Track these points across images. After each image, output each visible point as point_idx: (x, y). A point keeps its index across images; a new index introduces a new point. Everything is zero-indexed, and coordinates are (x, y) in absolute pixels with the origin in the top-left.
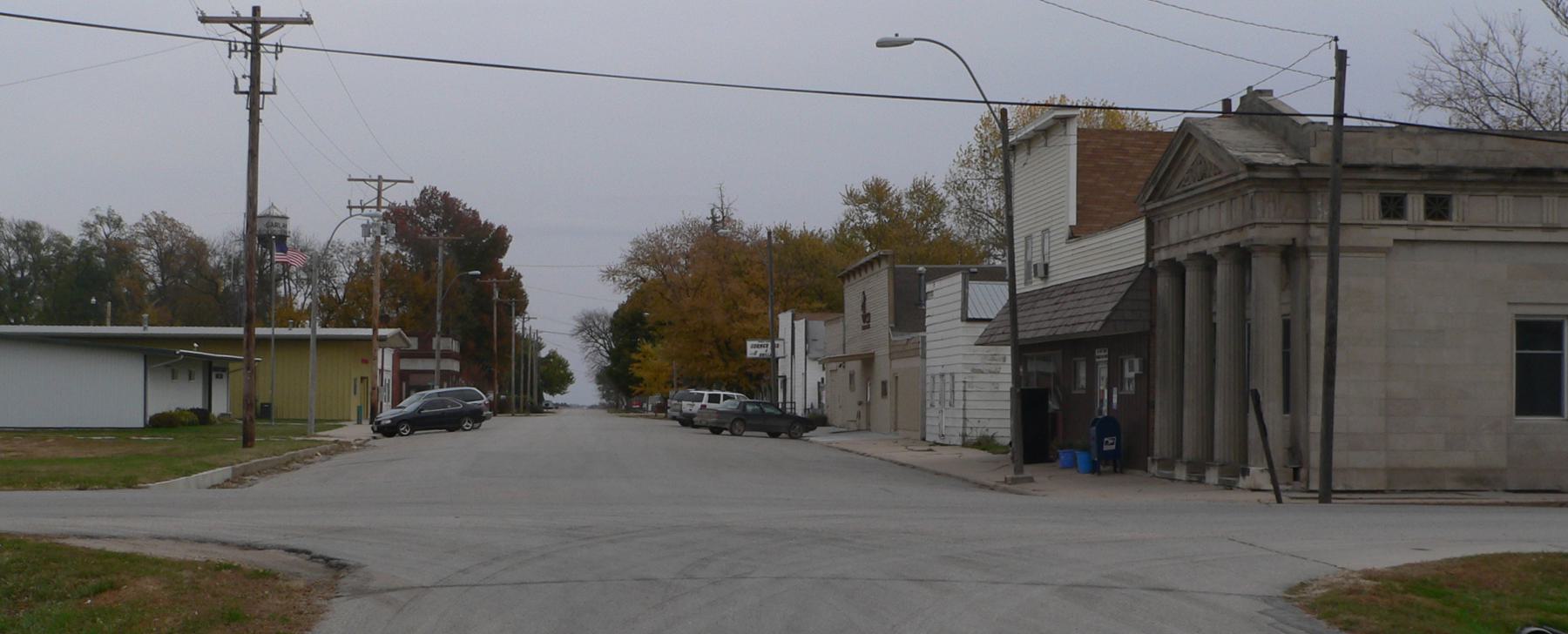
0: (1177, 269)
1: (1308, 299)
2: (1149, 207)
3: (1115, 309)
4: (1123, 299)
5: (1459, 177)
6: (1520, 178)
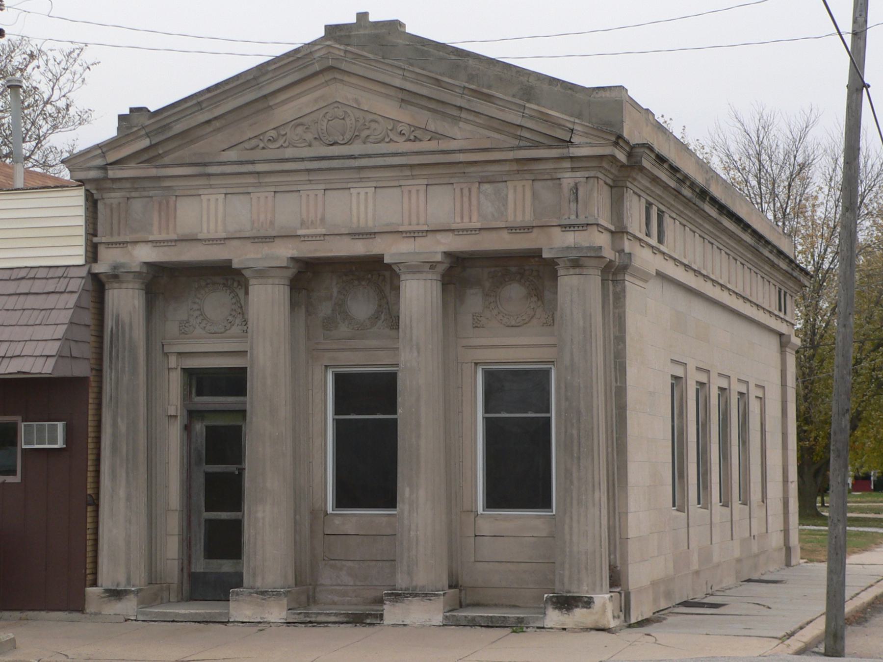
2: (111, 174)
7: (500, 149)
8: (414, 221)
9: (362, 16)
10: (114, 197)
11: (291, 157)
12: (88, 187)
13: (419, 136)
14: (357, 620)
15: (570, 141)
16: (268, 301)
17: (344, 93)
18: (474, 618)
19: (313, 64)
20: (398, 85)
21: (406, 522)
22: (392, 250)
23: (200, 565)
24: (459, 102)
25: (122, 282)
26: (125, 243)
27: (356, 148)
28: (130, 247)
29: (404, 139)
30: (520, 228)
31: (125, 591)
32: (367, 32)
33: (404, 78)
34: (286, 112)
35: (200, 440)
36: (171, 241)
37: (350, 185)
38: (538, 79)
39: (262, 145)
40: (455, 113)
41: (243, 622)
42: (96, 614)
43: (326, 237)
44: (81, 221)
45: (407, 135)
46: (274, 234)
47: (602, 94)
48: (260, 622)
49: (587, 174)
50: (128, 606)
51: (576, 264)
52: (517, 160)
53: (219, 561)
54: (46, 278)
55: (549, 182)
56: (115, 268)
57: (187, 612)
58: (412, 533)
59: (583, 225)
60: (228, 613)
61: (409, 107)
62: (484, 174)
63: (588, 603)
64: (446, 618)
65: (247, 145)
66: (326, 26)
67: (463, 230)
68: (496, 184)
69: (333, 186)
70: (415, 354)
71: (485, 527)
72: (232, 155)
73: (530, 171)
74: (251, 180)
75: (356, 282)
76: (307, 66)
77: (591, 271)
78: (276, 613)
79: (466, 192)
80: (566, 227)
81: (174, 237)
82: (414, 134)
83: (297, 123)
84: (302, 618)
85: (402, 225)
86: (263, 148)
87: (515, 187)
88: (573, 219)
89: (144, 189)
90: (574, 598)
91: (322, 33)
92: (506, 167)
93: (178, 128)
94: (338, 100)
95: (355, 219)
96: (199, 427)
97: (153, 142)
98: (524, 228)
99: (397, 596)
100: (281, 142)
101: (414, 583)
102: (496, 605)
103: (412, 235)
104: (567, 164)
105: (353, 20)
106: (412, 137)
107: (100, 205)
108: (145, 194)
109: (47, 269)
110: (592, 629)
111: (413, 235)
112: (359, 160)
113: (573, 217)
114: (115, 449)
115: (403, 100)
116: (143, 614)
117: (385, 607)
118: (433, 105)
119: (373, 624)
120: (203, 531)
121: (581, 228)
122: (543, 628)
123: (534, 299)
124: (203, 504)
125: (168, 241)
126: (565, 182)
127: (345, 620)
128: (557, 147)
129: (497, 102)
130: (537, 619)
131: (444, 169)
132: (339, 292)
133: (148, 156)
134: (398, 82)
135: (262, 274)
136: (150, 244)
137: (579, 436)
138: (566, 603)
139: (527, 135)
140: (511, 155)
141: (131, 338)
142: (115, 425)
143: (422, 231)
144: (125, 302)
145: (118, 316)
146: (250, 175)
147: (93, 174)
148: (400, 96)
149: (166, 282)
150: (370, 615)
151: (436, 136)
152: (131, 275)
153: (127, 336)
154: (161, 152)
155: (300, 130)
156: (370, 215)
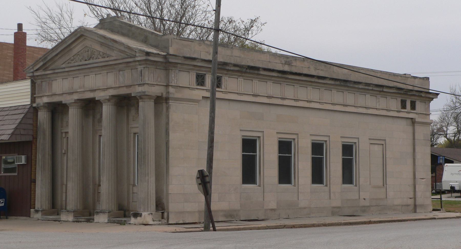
0: (57, 110)
1: (168, 124)
2: (36, 74)
3: (16, 128)
4: (20, 123)
5: (227, 68)
6: (248, 71)
23: (212, 229)
27: (91, 61)
33: (98, 37)
34: (75, 51)
44: (29, 90)
50: (39, 215)
64: (108, 220)
65: (67, 62)
77: (146, 100)
78: (71, 218)
80: (139, 85)
88: (141, 83)
92: (123, 65)
93: (49, 58)
111: (104, 90)
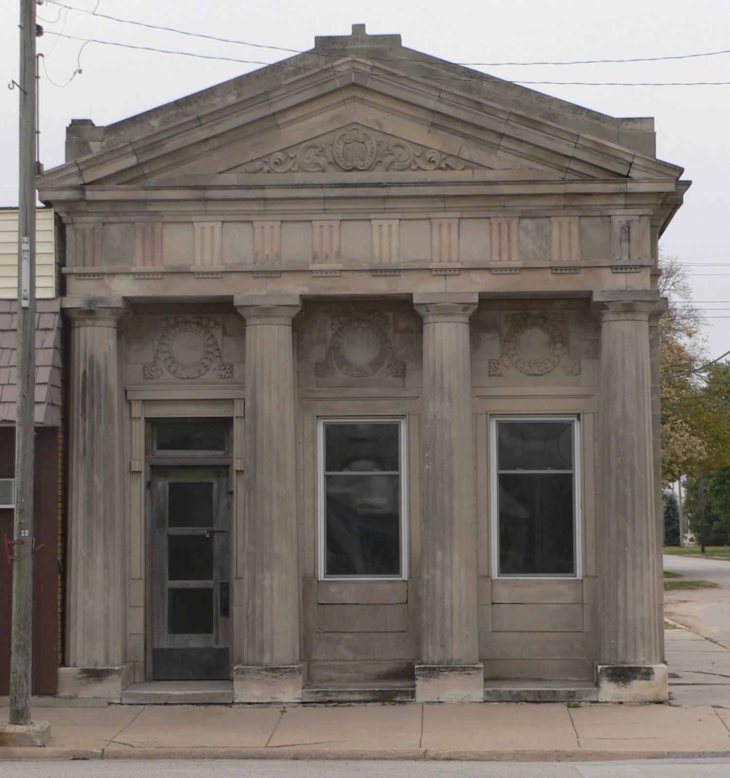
2: (89, 195)
7: (550, 182)
8: (445, 257)
9: (359, 28)
10: (87, 222)
11: (301, 182)
12: (58, 210)
13: (451, 164)
14: (385, 698)
15: (628, 176)
16: (270, 345)
17: (364, 113)
18: (519, 694)
19: (333, 80)
20: (432, 108)
21: (438, 589)
22: (423, 289)
23: (166, 641)
24: (503, 129)
25: (98, 319)
26: (101, 275)
27: (378, 175)
28: (106, 279)
29: (434, 167)
30: (566, 268)
31: (107, 670)
32: (364, 46)
33: (440, 100)
34: (295, 132)
35: (164, 500)
36: (157, 273)
37: (371, 216)
38: (562, 107)
39: (267, 168)
40: (494, 140)
41: (249, 704)
42: (71, 698)
43: (343, 274)
45: (437, 163)
46: (282, 268)
47: (633, 126)
48: (270, 703)
49: (640, 212)
50: (111, 688)
51: (629, 308)
52: (567, 195)
53: (187, 636)
54: (9, 313)
55: (597, 219)
56: (91, 302)
57: (182, 693)
58: (447, 601)
59: (635, 267)
60: (232, 694)
61: (441, 132)
62: (526, 208)
63: (647, 674)
64: (488, 693)
65: (249, 168)
66: (316, 38)
67: (501, 269)
68: (538, 220)
69: (292, 218)
70: (447, 404)
71: (504, 594)
72: (231, 178)
73: (578, 207)
74: (256, 207)
75: (356, 324)
76: (327, 82)
78: (290, 692)
79: (504, 227)
80: (617, 269)
81: (162, 269)
82: (446, 162)
83: (310, 144)
84: (320, 697)
85: (431, 262)
86: (268, 172)
87: (560, 223)
88: (625, 260)
89: (125, 213)
90: (631, 669)
91: (311, 45)
92: (553, 202)
94: (356, 121)
95: (377, 254)
96: (162, 484)
97: (140, 161)
98: (570, 268)
99: (432, 671)
100: (289, 166)
101: (449, 657)
102: (517, 679)
103: (443, 273)
104: (621, 201)
105: (348, 32)
106: (443, 166)
107: (69, 231)
108: (126, 219)
109: (9, 302)
110: (651, 702)
111: (444, 273)
112: (388, 189)
113: (626, 258)
114: (90, 509)
115: (433, 124)
116: (129, 696)
117: (417, 683)
118: (468, 131)
119: (404, 702)
120: (167, 602)
121: (633, 270)
122: (597, 702)
123: (559, 345)
124: (167, 572)
125: (153, 273)
126: (615, 220)
127: (371, 698)
128: (614, 182)
129: (546, 130)
130: (590, 693)
131: (486, 202)
132: (334, 335)
133: (130, 177)
134: (432, 104)
135: (266, 313)
136: (131, 276)
137: (633, 493)
138: (623, 674)
139: (574, 166)
140: (561, 189)
141: (106, 382)
142: (90, 481)
143: (455, 270)
144: (97, 341)
145: (92, 357)
146: (255, 200)
147: (66, 195)
148: (431, 120)
149: (142, 319)
150: (401, 692)
151: (470, 165)
152: (108, 312)
153: (103, 379)
154: (146, 172)
155: (312, 153)
156: (394, 251)
